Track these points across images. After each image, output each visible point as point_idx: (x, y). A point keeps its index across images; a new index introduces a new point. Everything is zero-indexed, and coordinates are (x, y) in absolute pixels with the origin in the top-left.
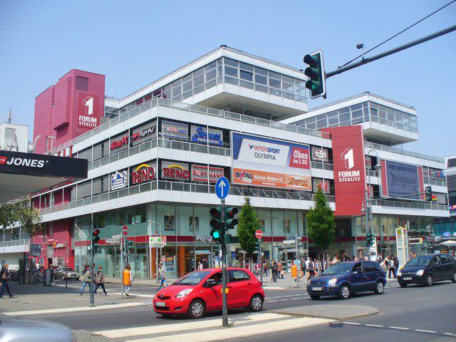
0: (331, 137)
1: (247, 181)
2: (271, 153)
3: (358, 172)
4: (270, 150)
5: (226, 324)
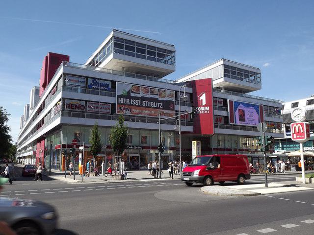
3: (208, 107)
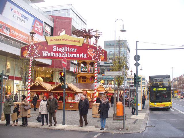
0: (54, 21)
1: (7, 33)
2: (23, 19)
4: (23, 16)
5: (139, 105)
